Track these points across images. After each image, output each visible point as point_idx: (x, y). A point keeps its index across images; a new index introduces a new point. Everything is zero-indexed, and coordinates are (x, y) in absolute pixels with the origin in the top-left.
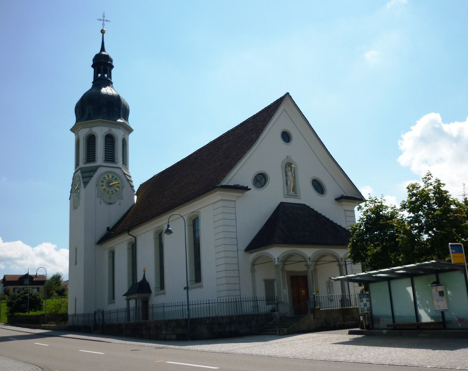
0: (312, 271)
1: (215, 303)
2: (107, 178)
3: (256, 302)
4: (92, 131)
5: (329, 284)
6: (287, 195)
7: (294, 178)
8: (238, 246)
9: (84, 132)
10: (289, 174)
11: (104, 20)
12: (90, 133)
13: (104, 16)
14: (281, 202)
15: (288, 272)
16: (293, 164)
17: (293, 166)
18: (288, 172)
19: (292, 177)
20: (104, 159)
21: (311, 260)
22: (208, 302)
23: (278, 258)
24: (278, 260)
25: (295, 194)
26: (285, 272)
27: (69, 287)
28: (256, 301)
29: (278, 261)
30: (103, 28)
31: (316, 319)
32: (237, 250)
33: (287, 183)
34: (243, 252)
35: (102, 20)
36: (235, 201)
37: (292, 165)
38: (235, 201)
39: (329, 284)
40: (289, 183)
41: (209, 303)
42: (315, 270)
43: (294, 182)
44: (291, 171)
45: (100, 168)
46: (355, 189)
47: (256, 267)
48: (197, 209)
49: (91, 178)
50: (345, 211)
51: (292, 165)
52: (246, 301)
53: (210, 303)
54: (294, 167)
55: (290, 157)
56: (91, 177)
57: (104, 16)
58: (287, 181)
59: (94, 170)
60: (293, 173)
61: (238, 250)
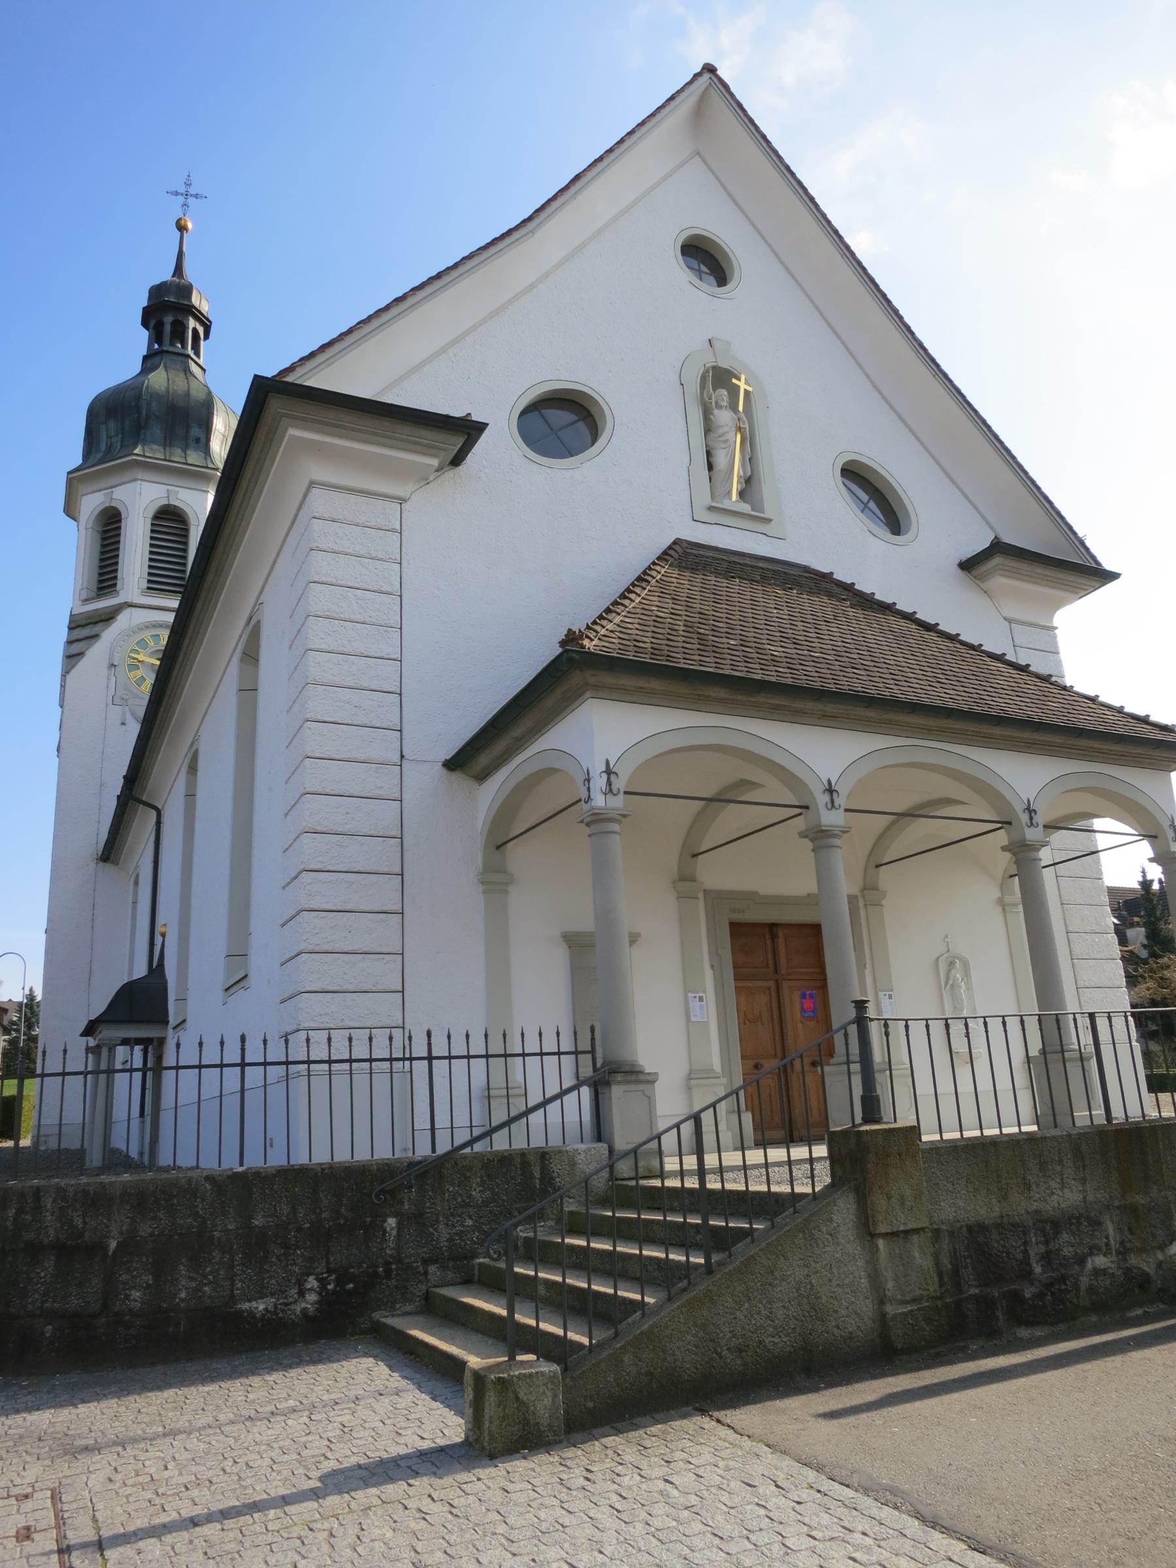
0: (852, 899)
1: (200, 1067)
2: (151, 644)
3: (421, 1067)
4: (112, 499)
5: (949, 971)
6: (711, 509)
7: (749, 442)
8: (403, 734)
9: (92, 503)
10: (723, 417)
11: (187, 195)
12: (108, 505)
13: (188, 185)
14: (677, 542)
15: (715, 898)
16: (743, 377)
17: (742, 385)
18: (716, 412)
19: (739, 436)
20: (145, 585)
21: (840, 801)
22: (233, 1056)
23: (609, 772)
24: (609, 783)
25: (753, 510)
26: (701, 895)
27: (41, 1004)
28: (137, 1070)
29: (609, 790)
30: (184, 215)
31: (881, 1243)
32: (396, 758)
33: (710, 467)
34: (438, 768)
35: (182, 194)
36: (402, 501)
37: (734, 381)
38: (402, 501)
39: (949, 971)
40: (721, 460)
41: (430, 1058)
42: (870, 894)
43: (751, 460)
44: (733, 407)
45: (130, 609)
46: (1053, 520)
47: (519, 857)
48: (254, 600)
49: (92, 645)
50: (1010, 621)
51: (739, 379)
52: (487, 1056)
53: (434, 1054)
54: (750, 389)
55: (728, 343)
56: (96, 637)
57: (188, 185)
58: (709, 454)
59: (108, 617)
60: (743, 416)
61: (402, 757)
